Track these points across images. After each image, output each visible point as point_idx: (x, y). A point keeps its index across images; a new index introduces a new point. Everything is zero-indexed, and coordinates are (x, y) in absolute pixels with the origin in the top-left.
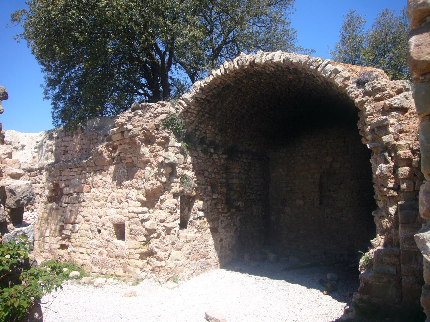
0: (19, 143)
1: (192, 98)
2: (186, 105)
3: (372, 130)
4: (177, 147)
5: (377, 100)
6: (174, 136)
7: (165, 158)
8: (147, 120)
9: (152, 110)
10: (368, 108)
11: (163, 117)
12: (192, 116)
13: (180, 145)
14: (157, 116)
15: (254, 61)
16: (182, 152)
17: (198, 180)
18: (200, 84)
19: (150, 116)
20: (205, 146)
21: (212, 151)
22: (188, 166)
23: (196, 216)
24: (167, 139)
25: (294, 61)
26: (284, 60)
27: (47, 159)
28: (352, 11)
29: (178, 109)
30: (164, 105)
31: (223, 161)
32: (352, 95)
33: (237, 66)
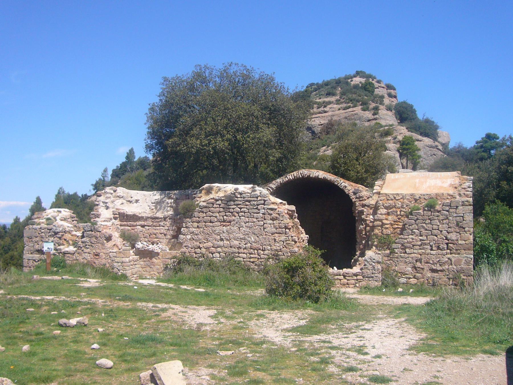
0: (132, 197)
3: (358, 212)
5: (360, 201)
10: (357, 204)
27: (168, 211)
32: (351, 198)
33: (301, 176)
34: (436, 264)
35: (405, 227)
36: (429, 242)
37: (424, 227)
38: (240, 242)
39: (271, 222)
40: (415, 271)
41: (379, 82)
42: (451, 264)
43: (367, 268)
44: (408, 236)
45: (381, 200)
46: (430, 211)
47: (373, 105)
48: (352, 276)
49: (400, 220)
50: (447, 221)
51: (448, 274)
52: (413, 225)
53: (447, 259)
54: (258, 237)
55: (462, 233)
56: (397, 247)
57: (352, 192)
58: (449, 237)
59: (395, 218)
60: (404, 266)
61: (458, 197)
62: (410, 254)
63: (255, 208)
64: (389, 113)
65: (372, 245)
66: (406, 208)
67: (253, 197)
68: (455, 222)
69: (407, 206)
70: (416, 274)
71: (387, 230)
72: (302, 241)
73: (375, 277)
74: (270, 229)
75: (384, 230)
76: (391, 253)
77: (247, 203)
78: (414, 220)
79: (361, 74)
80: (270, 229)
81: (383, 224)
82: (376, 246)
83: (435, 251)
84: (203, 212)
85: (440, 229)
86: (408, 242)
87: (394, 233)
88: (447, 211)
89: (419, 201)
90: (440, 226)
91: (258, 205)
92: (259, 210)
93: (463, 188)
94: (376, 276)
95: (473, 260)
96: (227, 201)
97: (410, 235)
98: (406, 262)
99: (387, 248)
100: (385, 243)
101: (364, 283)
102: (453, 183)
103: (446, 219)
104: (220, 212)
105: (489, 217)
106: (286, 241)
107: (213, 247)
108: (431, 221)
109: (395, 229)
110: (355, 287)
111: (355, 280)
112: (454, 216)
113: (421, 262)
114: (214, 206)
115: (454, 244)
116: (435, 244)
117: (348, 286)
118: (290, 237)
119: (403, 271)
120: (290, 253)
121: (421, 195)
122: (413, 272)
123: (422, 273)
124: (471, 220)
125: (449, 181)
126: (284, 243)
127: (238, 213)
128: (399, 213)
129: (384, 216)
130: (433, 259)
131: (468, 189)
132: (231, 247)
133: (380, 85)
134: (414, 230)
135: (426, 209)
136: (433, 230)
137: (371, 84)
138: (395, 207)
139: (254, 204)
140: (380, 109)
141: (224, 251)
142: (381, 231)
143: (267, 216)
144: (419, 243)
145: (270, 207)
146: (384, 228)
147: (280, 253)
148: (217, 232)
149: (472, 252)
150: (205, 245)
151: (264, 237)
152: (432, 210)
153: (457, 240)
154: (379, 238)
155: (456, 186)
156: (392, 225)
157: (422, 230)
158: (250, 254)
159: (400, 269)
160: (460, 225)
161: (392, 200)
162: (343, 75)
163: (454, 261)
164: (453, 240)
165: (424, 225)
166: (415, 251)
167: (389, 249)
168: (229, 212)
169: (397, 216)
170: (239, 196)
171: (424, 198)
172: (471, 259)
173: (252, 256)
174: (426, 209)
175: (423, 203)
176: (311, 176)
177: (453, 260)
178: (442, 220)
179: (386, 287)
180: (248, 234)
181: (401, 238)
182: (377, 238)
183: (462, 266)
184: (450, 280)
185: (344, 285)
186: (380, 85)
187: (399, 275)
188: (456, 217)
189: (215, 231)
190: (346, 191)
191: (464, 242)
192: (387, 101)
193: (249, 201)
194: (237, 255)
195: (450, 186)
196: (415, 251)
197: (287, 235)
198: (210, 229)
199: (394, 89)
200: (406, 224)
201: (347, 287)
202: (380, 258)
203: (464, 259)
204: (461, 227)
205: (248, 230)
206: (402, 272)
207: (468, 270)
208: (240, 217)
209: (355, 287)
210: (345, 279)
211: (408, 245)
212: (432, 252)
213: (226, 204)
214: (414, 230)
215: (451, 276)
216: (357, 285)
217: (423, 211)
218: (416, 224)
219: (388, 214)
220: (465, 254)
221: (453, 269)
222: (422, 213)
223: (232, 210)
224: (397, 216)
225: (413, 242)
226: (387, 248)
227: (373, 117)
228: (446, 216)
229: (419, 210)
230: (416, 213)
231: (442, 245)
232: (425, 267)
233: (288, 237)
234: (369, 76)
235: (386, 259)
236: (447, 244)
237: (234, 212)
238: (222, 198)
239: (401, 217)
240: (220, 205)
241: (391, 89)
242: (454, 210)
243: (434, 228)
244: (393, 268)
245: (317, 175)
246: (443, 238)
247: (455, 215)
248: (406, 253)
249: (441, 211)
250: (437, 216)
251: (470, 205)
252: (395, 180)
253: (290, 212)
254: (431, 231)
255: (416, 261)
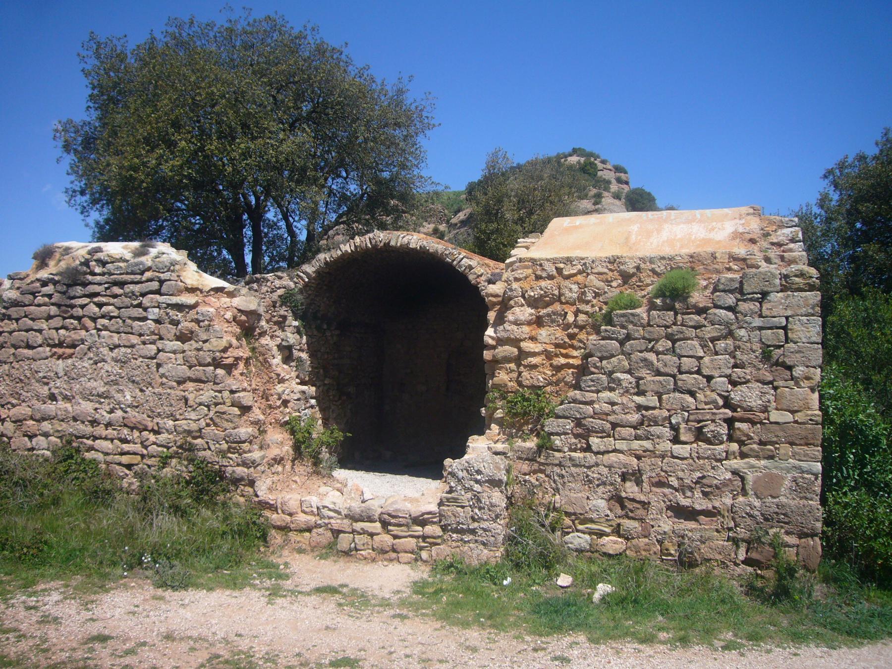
1: (314, 272)
2: (307, 280)
4: (295, 327)
6: (291, 314)
7: (283, 340)
8: (263, 296)
9: (269, 284)
11: (280, 292)
12: (310, 290)
13: (296, 323)
14: (274, 291)
15: (389, 243)
16: (299, 332)
17: (311, 363)
18: (325, 258)
19: (267, 292)
20: (319, 322)
21: (325, 327)
22: (303, 348)
23: (308, 405)
24: (284, 318)
25: (431, 251)
26: (420, 247)
28: (498, 149)
29: (296, 283)
30: (280, 278)
31: (335, 338)
34: (691, 489)
35: (587, 363)
36: (666, 414)
37: (652, 364)
38: (97, 406)
39: (177, 344)
40: (619, 512)
41: (604, 162)
42: (744, 492)
43: (455, 500)
44: (598, 392)
45: (517, 280)
46: (672, 308)
47: (594, 191)
48: (407, 525)
49: (575, 343)
50: (730, 342)
51: (732, 524)
52: (613, 356)
53: (728, 476)
54: (142, 391)
55: (781, 383)
56: (561, 430)
57: (485, 281)
58: (736, 396)
59: (560, 335)
60: (584, 495)
61: (763, 264)
62: (603, 453)
63: (135, 303)
64: (617, 202)
65: (491, 419)
66: (595, 301)
67: (133, 273)
68: (757, 346)
69: (597, 295)
70: (621, 521)
71: (534, 373)
72: (279, 403)
73: (480, 532)
74: (174, 367)
75: (525, 374)
76: (540, 448)
77: (116, 290)
78: (616, 339)
79: (578, 152)
80: (174, 367)
81: (523, 354)
82: (500, 423)
83: (688, 447)
84: (10, 318)
85: (706, 372)
86: (596, 415)
87: (557, 383)
88: (730, 309)
89: (634, 279)
90: (707, 359)
91: (143, 295)
92: (145, 309)
93: (773, 244)
94: (485, 530)
95: (819, 481)
96: (69, 286)
97: (605, 389)
98: (590, 482)
99: (532, 431)
100: (525, 413)
101: (443, 551)
102: (741, 230)
103: (725, 338)
104: (49, 317)
105: (848, 334)
106: (216, 404)
107: (32, 418)
108: (674, 342)
109: (558, 368)
110: (416, 560)
111: (417, 537)
112: (754, 325)
113: (639, 483)
114: (36, 302)
115: (753, 423)
116: (687, 421)
117: (394, 555)
118: (226, 394)
119: (579, 511)
120: (227, 442)
121: (640, 259)
122: (612, 516)
123: (641, 520)
124: (814, 339)
125: (729, 227)
126: (209, 410)
127: (94, 319)
128: (571, 318)
129: (526, 329)
130: (680, 474)
131: (792, 246)
132: (75, 419)
133: (605, 166)
134: (618, 375)
135: (658, 301)
136: (681, 373)
137: (592, 165)
138: (559, 299)
139: (133, 293)
140: (604, 197)
141: (58, 431)
142: (515, 375)
143: (168, 330)
144: (635, 417)
145: (174, 300)
146: (525, 366)
147: (199, 441)
148: (41, 375)
149: (817, 452)
150: (12, 413)
151: (156, 390)
152: (677, 305)
153: (765, 410)
154: (510, 396)
155: (755, 237)
156: (549, 356)
157: (643, 372)
158: (124, 441)
159: (571, 503)
160: (775, 357)
161: (550, 277)
162: (552, 154)
163: (755, 482)
164: (750, 410)
165: (652, 357)
166: (621, 445)
167: (538, 435)
168: (72, 317)
169: (567, 327)
170: (98, 270)
171: (653, 271)
172: (816, 475)
173: (126, 447)
174: (658, 301)
175: (648, 285)
176: (393, 243)
177: (750, 477)
178: (713, 340)
179: (518, 566)
180: (116, 383)
181: (575, 401)
182: (504, 398)
183: (783, 499)
184: (738, 547)
185: (383, 552)
186: (605, 166)
187: (567, 521)
188: (761, 328)
189: (36, 372)
190: (471, 277)
191: (789, 417)
192: (614, 187)
193: (122, 284)
194: (89, 442)
195: (734, 239)
196: (621, 445)
197: (218, 387)
198: (25, 365)
199: (626, 173)
200: (590, 355)
201: (391, 560)
202: (499, 469)
203: (789, 476)
204: (777, 364)
205: (118, 369)
206: (575, 514)
207: (803, 515)
208: (99, 330)
209: (416, 560)
210: (389, 532)
211: (597, 423)
212: (678, 449)
213: (64, 293)
214: (618, 375)
215: (742, 533)
216: (424, 555)
217: (649, 311)
218: (623, 353)
219: (539, 322)
220: (794, 456)
221: (748, 509)
222: (645, 316)
223: (78, 312)
224: (567, 327)
225: (614, 412)
226: (532, 431)
227: (593, 207)
228: (727, 324)
229: (634, 308)
230: (623, 315)
231: (712, 427)
232: (653, 499)
233: (220, 392)
234: (591, 155)
235: (525, 467)
236: (730, 422)
237: (84, 316)
238: (56, 278)
239: (576, 330)
240: (50, 296)
241: (621, 172)
242: (754, 306)
243: (684, 368)
244: (548, 498)
245: (405, 240)
246: (714, 402)
247: (758, 322)
248: (588, 449)
249: (709, 308)
250: (695, 327)
251: (812, 288)
252: (567, 230)
253: (243, 318)
254: (674, 376)
255: (624, 477)
